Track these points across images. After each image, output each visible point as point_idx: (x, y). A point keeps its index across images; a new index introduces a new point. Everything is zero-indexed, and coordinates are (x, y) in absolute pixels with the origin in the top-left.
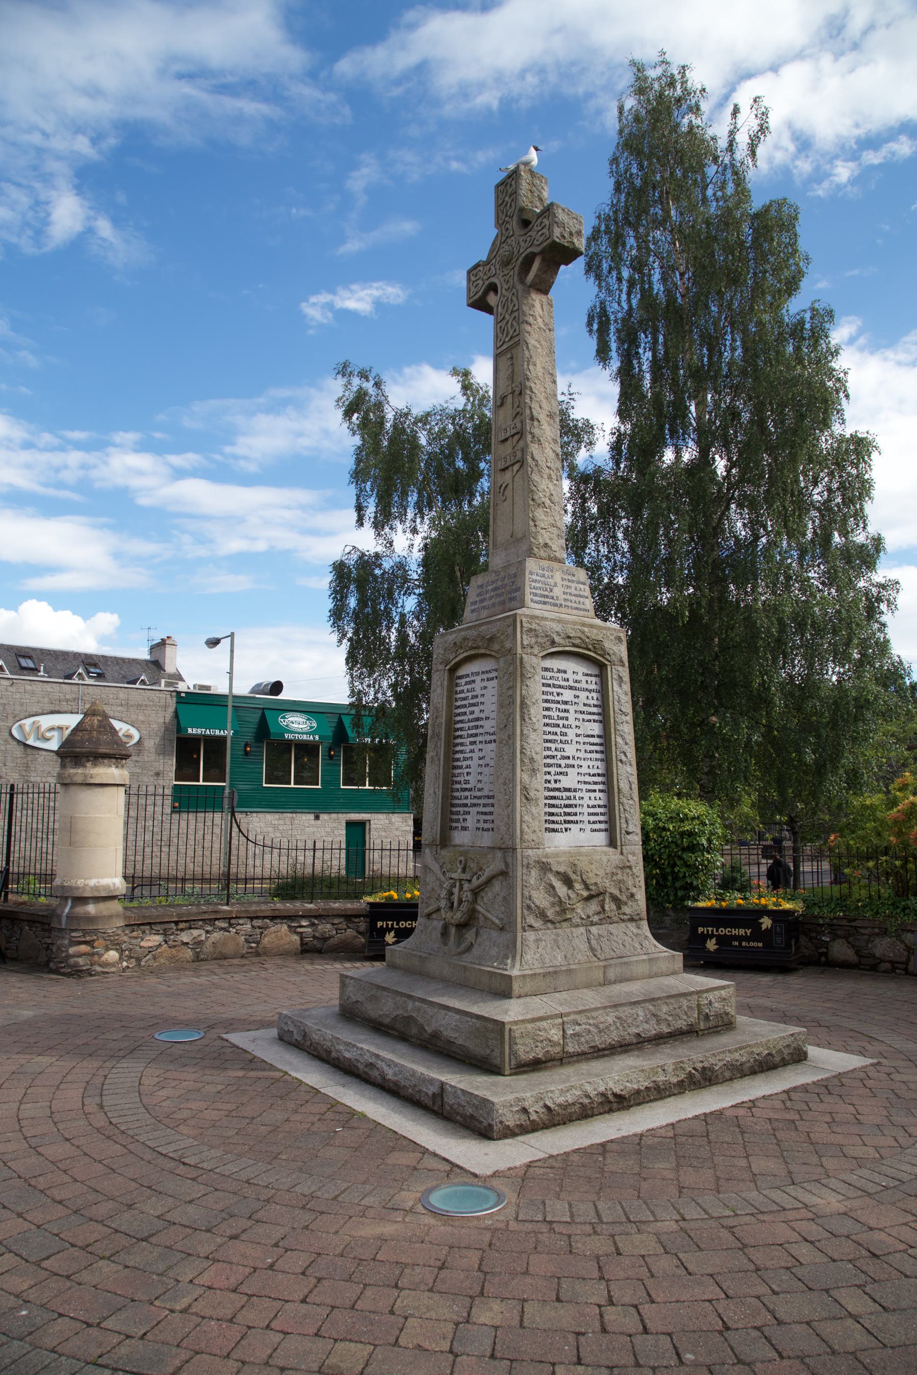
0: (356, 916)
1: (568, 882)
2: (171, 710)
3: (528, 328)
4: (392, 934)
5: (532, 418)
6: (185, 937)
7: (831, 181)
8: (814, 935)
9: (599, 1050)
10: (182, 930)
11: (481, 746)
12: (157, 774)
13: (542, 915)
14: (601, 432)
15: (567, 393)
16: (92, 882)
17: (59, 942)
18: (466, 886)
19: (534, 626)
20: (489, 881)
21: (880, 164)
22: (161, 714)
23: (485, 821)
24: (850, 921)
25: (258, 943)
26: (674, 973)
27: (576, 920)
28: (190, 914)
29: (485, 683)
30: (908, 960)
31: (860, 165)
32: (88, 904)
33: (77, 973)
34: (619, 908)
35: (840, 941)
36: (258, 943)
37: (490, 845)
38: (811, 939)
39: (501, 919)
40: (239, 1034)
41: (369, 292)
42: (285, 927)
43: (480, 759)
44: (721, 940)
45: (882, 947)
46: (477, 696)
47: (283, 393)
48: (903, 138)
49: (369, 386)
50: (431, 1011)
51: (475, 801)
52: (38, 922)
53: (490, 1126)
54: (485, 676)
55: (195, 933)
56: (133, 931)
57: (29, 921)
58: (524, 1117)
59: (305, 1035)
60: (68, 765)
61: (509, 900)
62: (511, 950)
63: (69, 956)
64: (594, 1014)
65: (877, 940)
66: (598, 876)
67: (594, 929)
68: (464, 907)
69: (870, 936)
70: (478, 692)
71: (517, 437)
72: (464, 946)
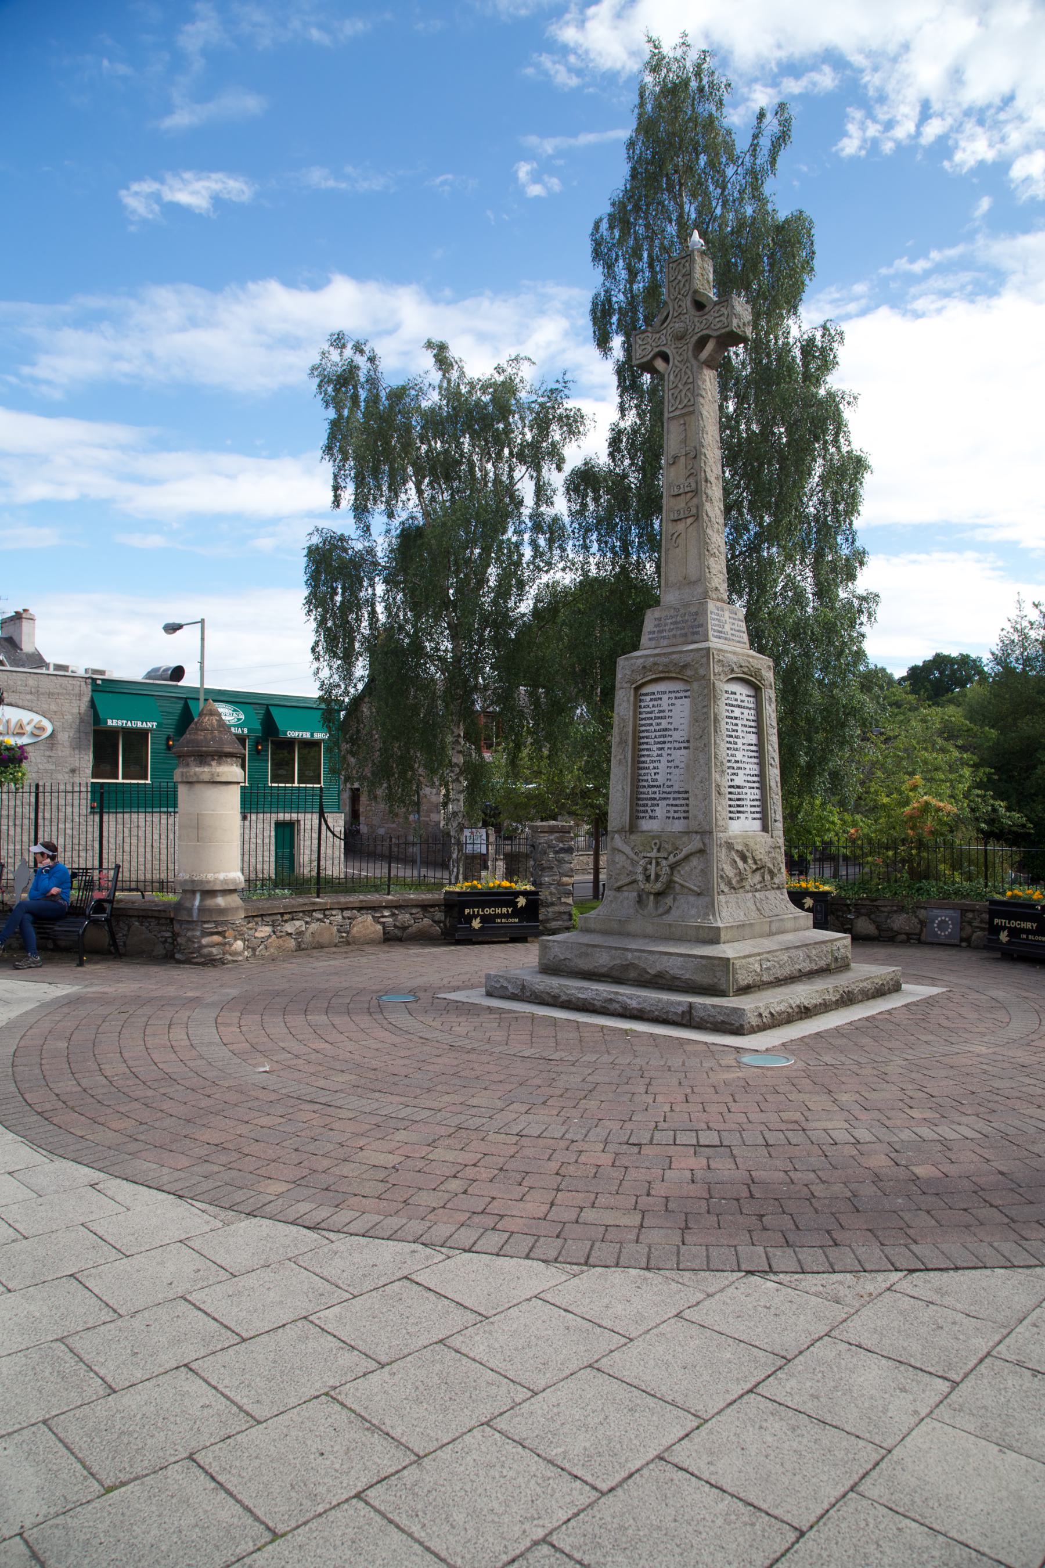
0: (432, 906)
1: (744, 859)
2: (86, 699)
3: (702, 400)
4: (478, 920)
5: (706, 481)
6: (289, 928)
7: (748, 107)
8: (840, 913)
9: (780, 980)
10: (286, 921)
11: (669, 752)
12: (73, 771)
13: (729, 883)
14: (592, 423)
15: (561, 380)
16: (222, 876)
17: (189, 934)
18: (664, 863)
19: (721, 658)
20: (687, 858)
21: (800, 95)
22: (76, 704)
23: (675, 812)
24: (873, 900)
25: (348, 933)
26: (808, 928)
27: (748, 888)
28: (293, 906)
29: (674, 701)
30: (921, 931)
31: (780, 92)
32: (216, 896)
33: (211, 962)
34: (772, 879)
35: (863, 918)
36: (348, 933)
37: (681, 830)
38: (838, 917)
39: (699, 887)
40: (463, 992)
41: (206, 184)
42: (370, 917)
43: (669, 762)
44: (1013, 933)
45: (900, 922)
46: (664, 711)
47: (94, 302)
48: (827, 69)
49: (361, 361)
50: (652, 958)
51: (665, 796)
52: (152, 917)
53: (742, 1026)
54: (673, 695)
55: (298, 923)
56: (249, 923)
57: (138, 917)
58: (760, 1020)
59: (523, 987)
60: (191, 764)
61: (706, 872)
62: (711, 908)
63: (202, 947)
64: (777, 954)
65: (895, 916)
66: (761, 854)
67: (757, 894)
68: (663, 879)
69: (889, 913)
70: (665, 707)
71: (689, 495)
72: (661, 910)
